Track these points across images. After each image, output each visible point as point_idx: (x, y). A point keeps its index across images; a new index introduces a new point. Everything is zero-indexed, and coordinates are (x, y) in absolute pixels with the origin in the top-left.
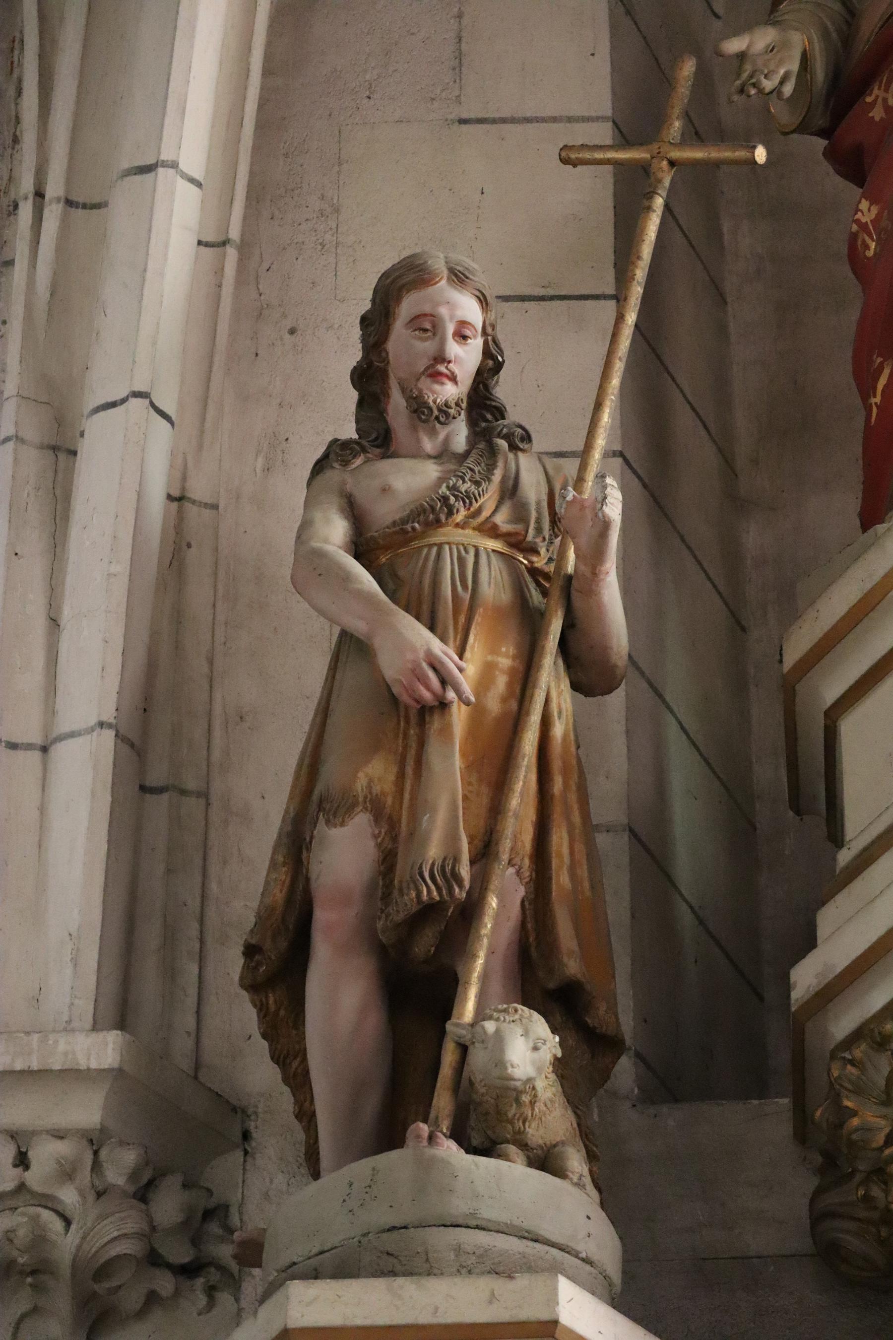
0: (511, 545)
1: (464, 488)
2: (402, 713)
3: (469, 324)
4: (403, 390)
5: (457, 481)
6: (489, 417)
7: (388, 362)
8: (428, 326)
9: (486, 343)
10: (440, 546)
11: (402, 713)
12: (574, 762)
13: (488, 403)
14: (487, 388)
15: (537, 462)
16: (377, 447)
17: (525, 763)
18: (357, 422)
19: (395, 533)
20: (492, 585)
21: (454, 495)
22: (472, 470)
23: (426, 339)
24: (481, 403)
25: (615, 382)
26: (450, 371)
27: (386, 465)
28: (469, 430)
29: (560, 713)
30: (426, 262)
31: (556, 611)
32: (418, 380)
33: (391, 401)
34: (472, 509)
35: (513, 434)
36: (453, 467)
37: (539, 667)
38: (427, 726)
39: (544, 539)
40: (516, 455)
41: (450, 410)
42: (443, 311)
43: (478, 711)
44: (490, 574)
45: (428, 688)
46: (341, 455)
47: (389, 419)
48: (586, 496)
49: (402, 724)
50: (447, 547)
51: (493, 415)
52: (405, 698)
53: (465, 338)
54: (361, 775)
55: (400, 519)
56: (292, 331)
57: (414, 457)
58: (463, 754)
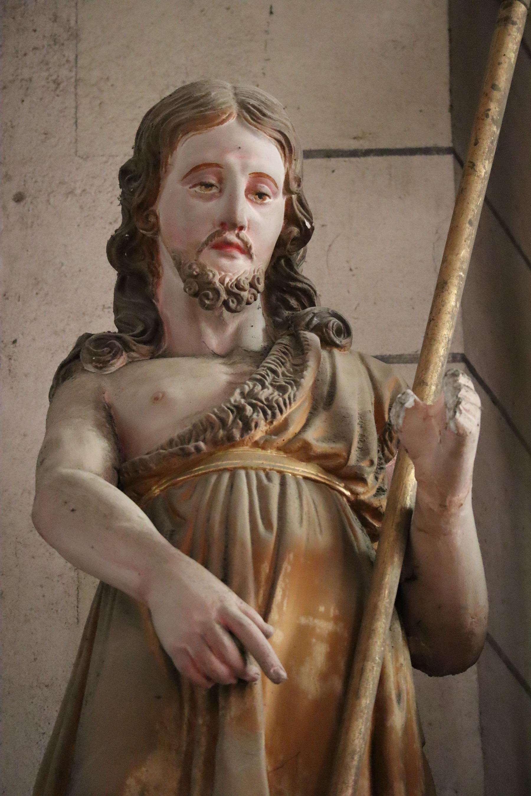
0: (328, 470)
2: (186, 696)
3: (268, 177)
4: (179, 266)
5: (254, 386)
6: (293, 302)
8: (213, 180)
9: (289, 205)
10: (233, 472)
11: (186, 696)
12: (419, 764)
13: (292, 284)
14: (290, 264)
15: (359, 363)
16: (145, 343)
18: (117, 310)
19: (172, 455)
20: (305, 523)
21: (251, 405)
22: (274, 372)
23: (210, 198)
24: (284, 286)
25: (465, 252)
26: (242, 240)
27: (158, 366)
28: (267, 321)
30: (208, 94)
31: (392, 557)
32: (200, 251)
33: (163, 281)
34: (275, 423)
35: (326, 325)
36: (246, 368)
37: (371, 633)
38: (221, 713)
39: (372, 463)
40: (330, 352)
41: (243, 293)
42: (233, 159)
43: (289, 692)
44: (301, 505)
45: (224, 660)
46: (95, 354)
48: (429, 403)
49: (186, 711)
50: (243, 473)
51: (298, 300)
53: (262, 195)
54: (131, 782)
55: (179, 437)
56: (19, 198)
57: (194, 355)
58: (270, 752)
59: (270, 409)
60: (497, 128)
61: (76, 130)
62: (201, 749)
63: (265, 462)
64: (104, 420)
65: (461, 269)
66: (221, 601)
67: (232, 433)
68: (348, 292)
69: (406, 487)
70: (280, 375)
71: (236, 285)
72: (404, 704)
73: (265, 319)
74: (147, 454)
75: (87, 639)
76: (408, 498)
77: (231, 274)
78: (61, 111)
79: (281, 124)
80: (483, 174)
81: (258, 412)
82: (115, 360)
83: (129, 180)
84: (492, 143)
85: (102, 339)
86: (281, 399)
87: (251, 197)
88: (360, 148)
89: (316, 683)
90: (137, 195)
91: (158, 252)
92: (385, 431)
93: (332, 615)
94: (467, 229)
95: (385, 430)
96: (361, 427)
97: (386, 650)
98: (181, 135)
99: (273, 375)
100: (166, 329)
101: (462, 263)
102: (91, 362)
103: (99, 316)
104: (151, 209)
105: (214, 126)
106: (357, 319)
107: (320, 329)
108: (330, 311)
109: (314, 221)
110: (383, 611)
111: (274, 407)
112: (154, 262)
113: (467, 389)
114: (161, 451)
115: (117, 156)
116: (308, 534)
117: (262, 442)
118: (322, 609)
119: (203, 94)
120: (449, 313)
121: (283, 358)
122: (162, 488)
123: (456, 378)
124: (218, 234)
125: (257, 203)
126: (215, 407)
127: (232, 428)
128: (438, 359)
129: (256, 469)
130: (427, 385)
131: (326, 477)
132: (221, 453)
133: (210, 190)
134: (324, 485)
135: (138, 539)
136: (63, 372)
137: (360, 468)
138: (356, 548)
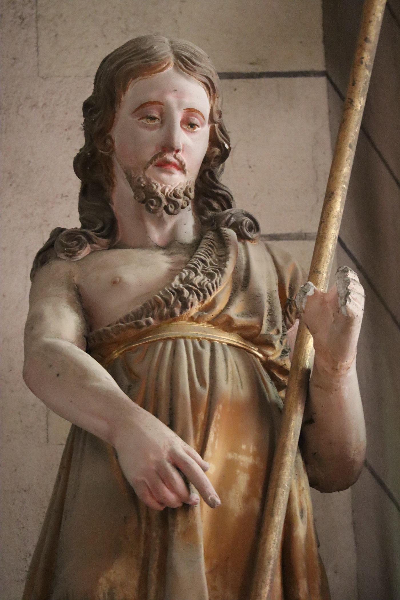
0: (245, 338)
1: (198, 279)
2: (143, 514)
3: (198, 111)
4: (130, 179)
5: (190, 273)
6: (215, 205)
7: (114, 151)
8: (156, 114)
9: (212, 131)
10: (175, 341)
11: (143, 514)
12: (316, 562)
13: (215, 191)
14: (213, 176)
16: (104, 237)
17: (271, 566)
18: (81, 210)
19: (130, 327)
22: (203, 262)
24: (208, 192)
26: (178, 160)
27: (115, 256)
28: (195, 219)
29: (302, 512)
31: (296, 407)
32: (145, 168)
33: (116, 189)
34: (206, 302)
35: (241, 224)
37: (281, 466)
38: (170, 529)
39: (278, 332)
40: (244, 244)
42: (171, 99)
43: (219, 512)
45: (172, 489)
47: (114, 208)
49: (143, 526)
50: (182, 341)
51: (219, 202)
52: (150, 501)
53: (193, 126)
54: (102, 581)
55: (133, 313)
58: (207, 558)
59: (202, 292)
60: (369, 72)
61: (38, 56)
62: (155, 557)
63: (198, 333)
64: (75, 298)
65: (344, 182)
66: (171, 445)
67: (174, 311)
68: (249, 184)
69: (305, 352)
70: (209, 264)
71: (174, 194)
72: (305, 519)
73: (194, 217)
74: (109, 326)
75: (64, 467)
76: (307, 361)
77: (169, 186)
78: (26, 41)
79: (207, 71)
80: (359, 108)
81: (193, 294)
82: (82, 251)
83: (91, 111)
84: (365, 83)
85: (72, 234)
86: (210, 284)
87: (185, 127)
88: (255, 71)
89: (241, 504)
90: (97, 123)
91: (112, 166)
92: (287, 305)
93: (251, 451)
94: (348, 152)
95: (287, 304)
96: (269, 303)
97: (292, 479)
98: (131, 80)
99: (203, 264)
100: (119, 225)
101: (345, 177)
102: (63, 252)
103: (59, 203)
104: (108, 134)
105: (157, 73)
106: (255, 205)
107: (236, 226)
108: (243, 212)
109: (231, 143)
110: (290, 448)
111: (204, 290)
112: (110, 174)
113: (355, 283)
114: (120, 324)
115: (70, 77)
116: (233, 389)
117: (196, 317)
118: (244, 447)
119: (148, 47)
120: (336, 217)
121: (209, 250)
122: (121, 352)
123: (346, 274)
124: (161, 154)
125: (190, 132)
126: (159, 290)
127: (174, 307)
128: (328, 253)
129: (192, 339)
130: (320, 273)
131: (244, 344)
132: (165, 326)
133: (154, 122)
134: (243, 350)
135: (107, 396)
136: (40, 258)
137: (270, 336)
138: (268, 398)
